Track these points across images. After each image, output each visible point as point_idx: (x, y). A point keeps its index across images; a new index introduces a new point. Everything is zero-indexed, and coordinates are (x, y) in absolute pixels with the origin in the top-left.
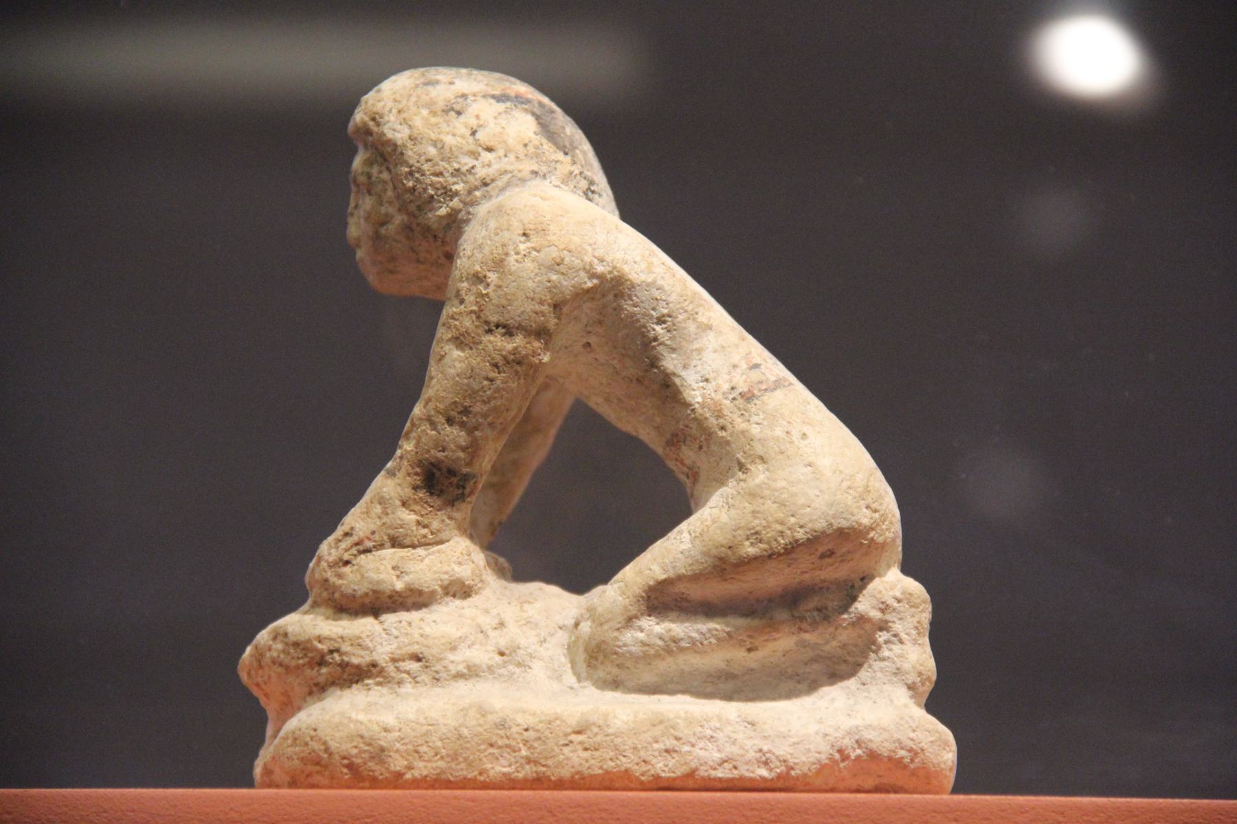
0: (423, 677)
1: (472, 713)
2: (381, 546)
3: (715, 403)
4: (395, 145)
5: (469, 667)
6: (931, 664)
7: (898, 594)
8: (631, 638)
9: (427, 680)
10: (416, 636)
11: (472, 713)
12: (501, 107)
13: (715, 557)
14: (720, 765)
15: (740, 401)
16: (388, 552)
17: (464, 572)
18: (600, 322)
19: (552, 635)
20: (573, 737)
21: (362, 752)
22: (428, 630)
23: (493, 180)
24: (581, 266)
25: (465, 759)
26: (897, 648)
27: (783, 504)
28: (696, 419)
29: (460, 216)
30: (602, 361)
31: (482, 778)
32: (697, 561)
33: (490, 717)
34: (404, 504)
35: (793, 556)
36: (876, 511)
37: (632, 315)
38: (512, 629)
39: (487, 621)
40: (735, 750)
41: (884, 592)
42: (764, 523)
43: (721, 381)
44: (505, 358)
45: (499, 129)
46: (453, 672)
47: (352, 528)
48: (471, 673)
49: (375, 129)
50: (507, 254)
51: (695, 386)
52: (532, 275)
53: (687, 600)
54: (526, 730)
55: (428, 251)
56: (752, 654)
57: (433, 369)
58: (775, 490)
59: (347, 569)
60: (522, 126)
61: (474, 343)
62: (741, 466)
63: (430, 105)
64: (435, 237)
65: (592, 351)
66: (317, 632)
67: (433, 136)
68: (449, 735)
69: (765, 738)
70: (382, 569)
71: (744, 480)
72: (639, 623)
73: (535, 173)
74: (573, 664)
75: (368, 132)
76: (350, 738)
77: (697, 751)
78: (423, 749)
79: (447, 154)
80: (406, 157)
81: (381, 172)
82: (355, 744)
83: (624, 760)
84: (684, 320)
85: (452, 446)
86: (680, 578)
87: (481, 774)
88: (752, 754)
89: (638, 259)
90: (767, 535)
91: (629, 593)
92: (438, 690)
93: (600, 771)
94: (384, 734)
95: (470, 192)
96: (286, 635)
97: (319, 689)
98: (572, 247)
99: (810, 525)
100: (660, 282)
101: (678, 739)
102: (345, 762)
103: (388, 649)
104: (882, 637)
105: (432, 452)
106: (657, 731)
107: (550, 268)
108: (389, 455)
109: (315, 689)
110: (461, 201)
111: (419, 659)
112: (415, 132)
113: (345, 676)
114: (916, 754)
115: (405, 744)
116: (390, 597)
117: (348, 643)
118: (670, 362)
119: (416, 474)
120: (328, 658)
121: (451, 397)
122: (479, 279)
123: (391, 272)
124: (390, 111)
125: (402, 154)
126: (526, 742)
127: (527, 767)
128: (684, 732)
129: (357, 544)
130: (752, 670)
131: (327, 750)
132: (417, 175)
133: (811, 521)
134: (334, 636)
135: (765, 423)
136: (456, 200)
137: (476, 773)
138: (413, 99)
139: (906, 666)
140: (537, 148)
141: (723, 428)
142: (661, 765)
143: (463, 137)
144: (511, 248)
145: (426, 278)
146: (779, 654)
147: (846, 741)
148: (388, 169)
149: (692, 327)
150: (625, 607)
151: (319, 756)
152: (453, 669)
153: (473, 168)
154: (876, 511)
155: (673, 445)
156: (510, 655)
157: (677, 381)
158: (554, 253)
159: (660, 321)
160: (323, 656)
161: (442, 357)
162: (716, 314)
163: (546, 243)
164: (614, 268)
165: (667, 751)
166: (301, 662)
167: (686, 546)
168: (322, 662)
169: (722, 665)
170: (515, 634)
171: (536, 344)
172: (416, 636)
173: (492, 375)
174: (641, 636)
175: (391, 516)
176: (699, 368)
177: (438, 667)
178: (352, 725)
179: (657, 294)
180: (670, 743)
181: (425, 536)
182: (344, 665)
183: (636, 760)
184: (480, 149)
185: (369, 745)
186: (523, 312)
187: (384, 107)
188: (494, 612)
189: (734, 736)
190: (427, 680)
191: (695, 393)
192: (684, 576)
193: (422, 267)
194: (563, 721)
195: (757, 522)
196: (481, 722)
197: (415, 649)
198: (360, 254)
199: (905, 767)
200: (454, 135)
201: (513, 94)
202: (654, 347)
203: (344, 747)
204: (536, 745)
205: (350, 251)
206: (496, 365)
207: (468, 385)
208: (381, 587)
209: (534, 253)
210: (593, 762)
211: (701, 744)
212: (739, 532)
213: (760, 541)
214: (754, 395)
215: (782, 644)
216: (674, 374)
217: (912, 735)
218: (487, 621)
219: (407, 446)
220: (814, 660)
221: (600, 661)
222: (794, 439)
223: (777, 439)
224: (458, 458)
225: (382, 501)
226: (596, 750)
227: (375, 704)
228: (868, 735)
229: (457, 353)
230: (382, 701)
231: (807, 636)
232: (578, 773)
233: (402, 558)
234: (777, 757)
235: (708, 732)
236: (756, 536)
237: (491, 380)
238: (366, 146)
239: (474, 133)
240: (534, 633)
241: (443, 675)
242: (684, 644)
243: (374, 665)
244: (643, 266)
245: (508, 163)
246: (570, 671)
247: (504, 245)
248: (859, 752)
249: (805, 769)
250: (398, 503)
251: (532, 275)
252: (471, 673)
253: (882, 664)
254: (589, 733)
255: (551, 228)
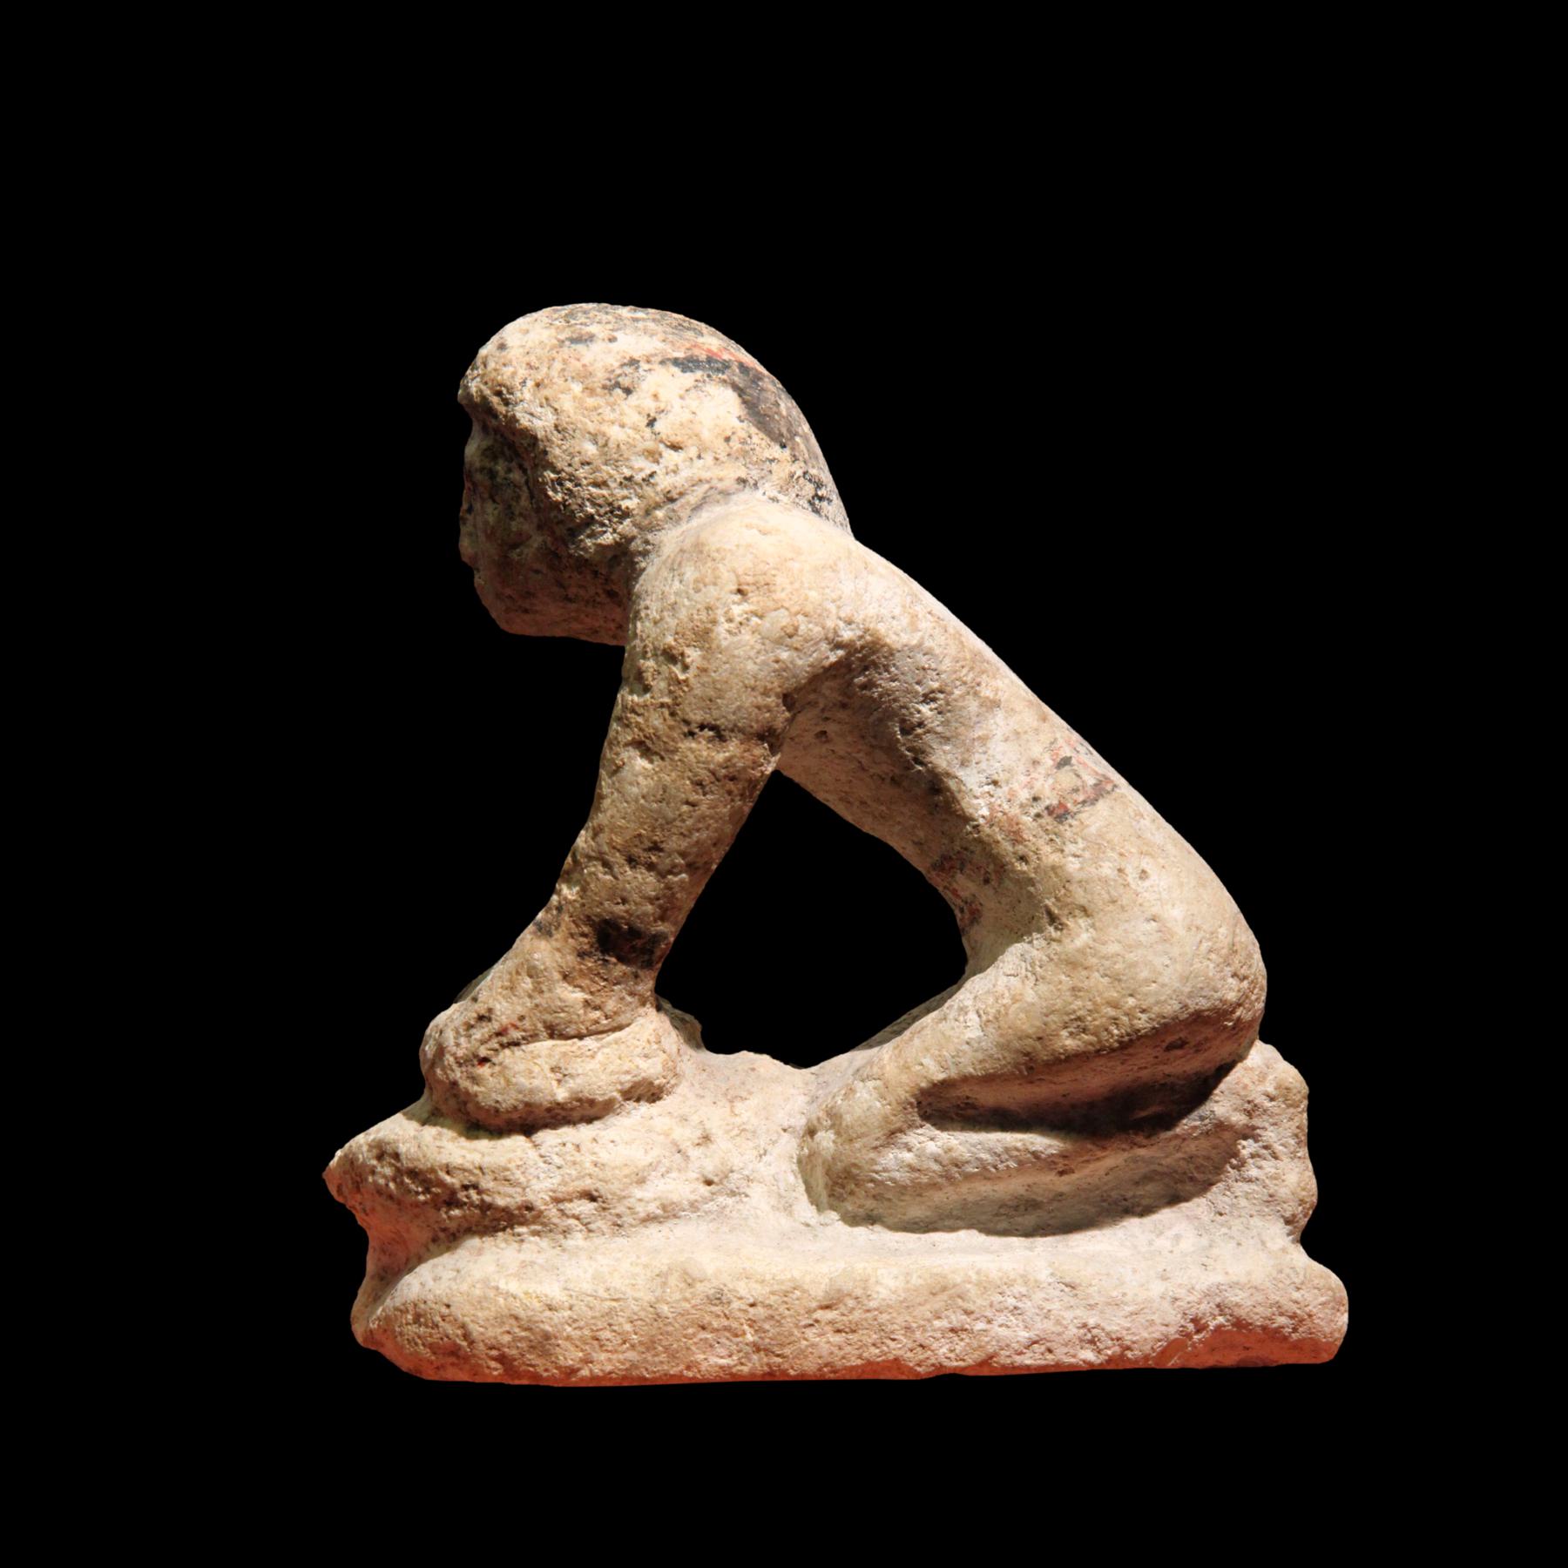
0: (600, 1224)
1: (673, 1280)
2: (533, 1037)
3: (1010, 820)
4: (535, 438)
5: (664, 1207)
6: (1312, 1184)
7: (1271, 1090)
8: (893, 1162)
9: (604, 1228)
10: (588, 1165)
11: (673, 1280)
12: (688, 379)
13: (1017, 1051)
14: (1027, 1347)
15: (1047, 820)
16: (545, 1046)
17: (651, 1068)
18: (844, 706)
19: (774, 1143)
20: (819, 1314)
21: (516, 1339)
22: (604, 1156)
23: (681, 494)
24: (822, 635)
25: (666, 1349)
26: (1269, 1166)
27: (1116, 979)
28: (980, 841)
29: (633, 546)
30: (842, 753)
31: (690, 1374)
32: (991, 1056)
33: (700, 1287)
34: (565, 977)
35: (1131, 1051)
36: (1245, 978)
37: (887, 693)
38: (722, 1143)
39: (686, 1135)
40: (1049, 1326)
41: (1251, 1087)
42: (1089, 1005)
43: (1016, 786)
44: (713, 773)
45: (687, 416)
46: (642, 1215)
47: (490, 1010)
48: (668, 1213)
49: (502, 409)
50: (714, 622)
51: (978, 791)
52: (752, 654)
53: (974, 1107)
54: (752, 1305)
55: (581, 586)
56: (1065, 1178)
57: (605, 784)
58: (1106, 958)
59: (485, 1071)
60: (718, 408)
61: (667, 751)
62: (1053, 919)
63: (584, 375)
64: (596, 573)
65: (827, 741)
66: (444, 1159)
67: (591, 427)
68: (642, 1314)
69: (1091, 1307)
70: (534, 1070)
71: (1059, 941)
72: (904, 1139)
73: (742, 481)
74: (809, 1190)
75: (490, 411)
76: (500, 1319)
77: (996, 1329)
78: (606, 1334)
79: (611, 453)
80: (550, 458)
81: (509, 470)
82: (507, 1328)
83: (892, 1344)
84: (962, 696)
85: (636, 897)
86: (966, 1079)
87: (688, 1368)
88: (1073, 1331)
89: (897, 612)
90: (1091, 1022)
91: (891, 1098)
92: (620, 1240)
93: (859, 1362)
94: (548, 1313)
95: (648, 513)
96: (396, 1156)
97: (449, 1239)
98: (809, 608)
99: (1156, 1009)
100: (928, 644)
101: (968, 1313)
102: (494, 1353)
103: (548, 1184)
104: (1247, 1147)
105: (606, 904)
106: (938, 1303)
107: (779, 642)
108: (542, 902)
109: (442, 1235)
110: (635, 525)
111: (593, 1199)
112: (564, 419)
113: (486, 1222)
114: (1301, 1321)
115: (580, 1328)
116: (549, 1110)
117: (489, 1177)
118: (942, 758)
119: (584, 935)
120: (462, 1195)
121: (633, 828)
122: (671, 656)
123: (526, 611)
124: (524, 383)
125: (545, 453)
126: (752, 1323)
127: (755, 1357)
128: (978, 1302)
129: (498, 1034)
130: (1061, 1194)
131: (466, 1336)
132: (569, 485)
133: (1157, 1003)
134: (468, 1165)
135: (1087, 855)
136: (627, 522)
137: (682, 1367)
138: (558, 365)
139: (1283, 1192)
140: (744, 442)
141: (1023, 858)
142: (944, 1350)
143: (636, 429)
144: (720, 612)
145: (576, 619)
146: (1102, 1172)
147: (1204, 1307)
148: (521, 467)
149: (973, 706)
150: (886, 1118)
151: (455, 1344)
152: (642, 1210)
153: (652, 475)
154: (1245, 978)
155: (943, 870)
156: (721, 1182)
157: (952, 784)
158: (783, 619)
159: (928, 698)
160: (453, 1192)
161: (618, 769)
162: (1006, 683)
163: (771, 604)
164: (867, 630)
165: (952, 1330)
166: (422, 1198)
167: (974, 1033)
168: (452, 1201)
169: (1022, 1191)
170: (727, 1152)
171: (758, 751)
172: (588, 1165)
173: (694, 797)
174: (908, 1157)
175: (547, 995)
176: (983, 765)
177: (620, 1209)
178: (501, 1300)
179: (923, 661)
180: (957, 1319)
181: (597, 1022)
182: (485, 1207)
183: (910, 1345)
184: (662, 447)
185: (528, 1329)
186: (739, 708)
187: (514, 374)
188: (695, 1119)
189: (1048, 1306)
190: (604, 1228)
191: (979, 804)
192: (972, 1077)
193: (573, 606)
194: (804, 1291)
195: (1079, 1003)
196: (688, 1295)
197: (587, 1184)
198: (479, 580)
199: (1285, 1338)
200: (622, 426)
201: (703, 357)
202: (918, 736)
203: (491, 1333)
204: (767, 1327)
205: (467, 572)
206: (700, 784)
207: (659, 811)
208: (537, 1098)
209: (755, 620)
210: (848, 1349)
211: (1001, 1319)
212: (1052, 1017)
213: (1084, 1031)
214: (1067, 812)
215: (1110, 1163)
216: (948, 775)
217: (1296, 1295)
218: (686, 1135)
219: (567, 892)
220: (1148, 1178)
221: (845, 1189)
222: (1130, 879)
223: (1105, 881)
224: (645, 914)
225: (532, 973)
226: (854, 1331)
227: (532, 1263)
228: (1235, 1297)
229: (641, 763)
230: (541, 1260)
231: (1142, 1152)
232: (826, 1365)
233: (565, 1054)
234: (1108, 1334)
235: (1011, 1302)
236: (1078, 1024)
237: (693, 805)
238: (485, 428)
239: (651, 423)
240: (751, 1144)
241: (628, 1219)
242: (970, 1169)
243: (529, 1208)
244: (905, 621)
245: (703, 469)
246: (805, 1198)
247: (708, 608)
248: (1221, 1320)
249: (1147, 1349)
250: (557, 976)
251: (752, 654)
252: (668, 1213)
253: (1246, 1187)
254: (843, 1309)
255: (779, 580)
